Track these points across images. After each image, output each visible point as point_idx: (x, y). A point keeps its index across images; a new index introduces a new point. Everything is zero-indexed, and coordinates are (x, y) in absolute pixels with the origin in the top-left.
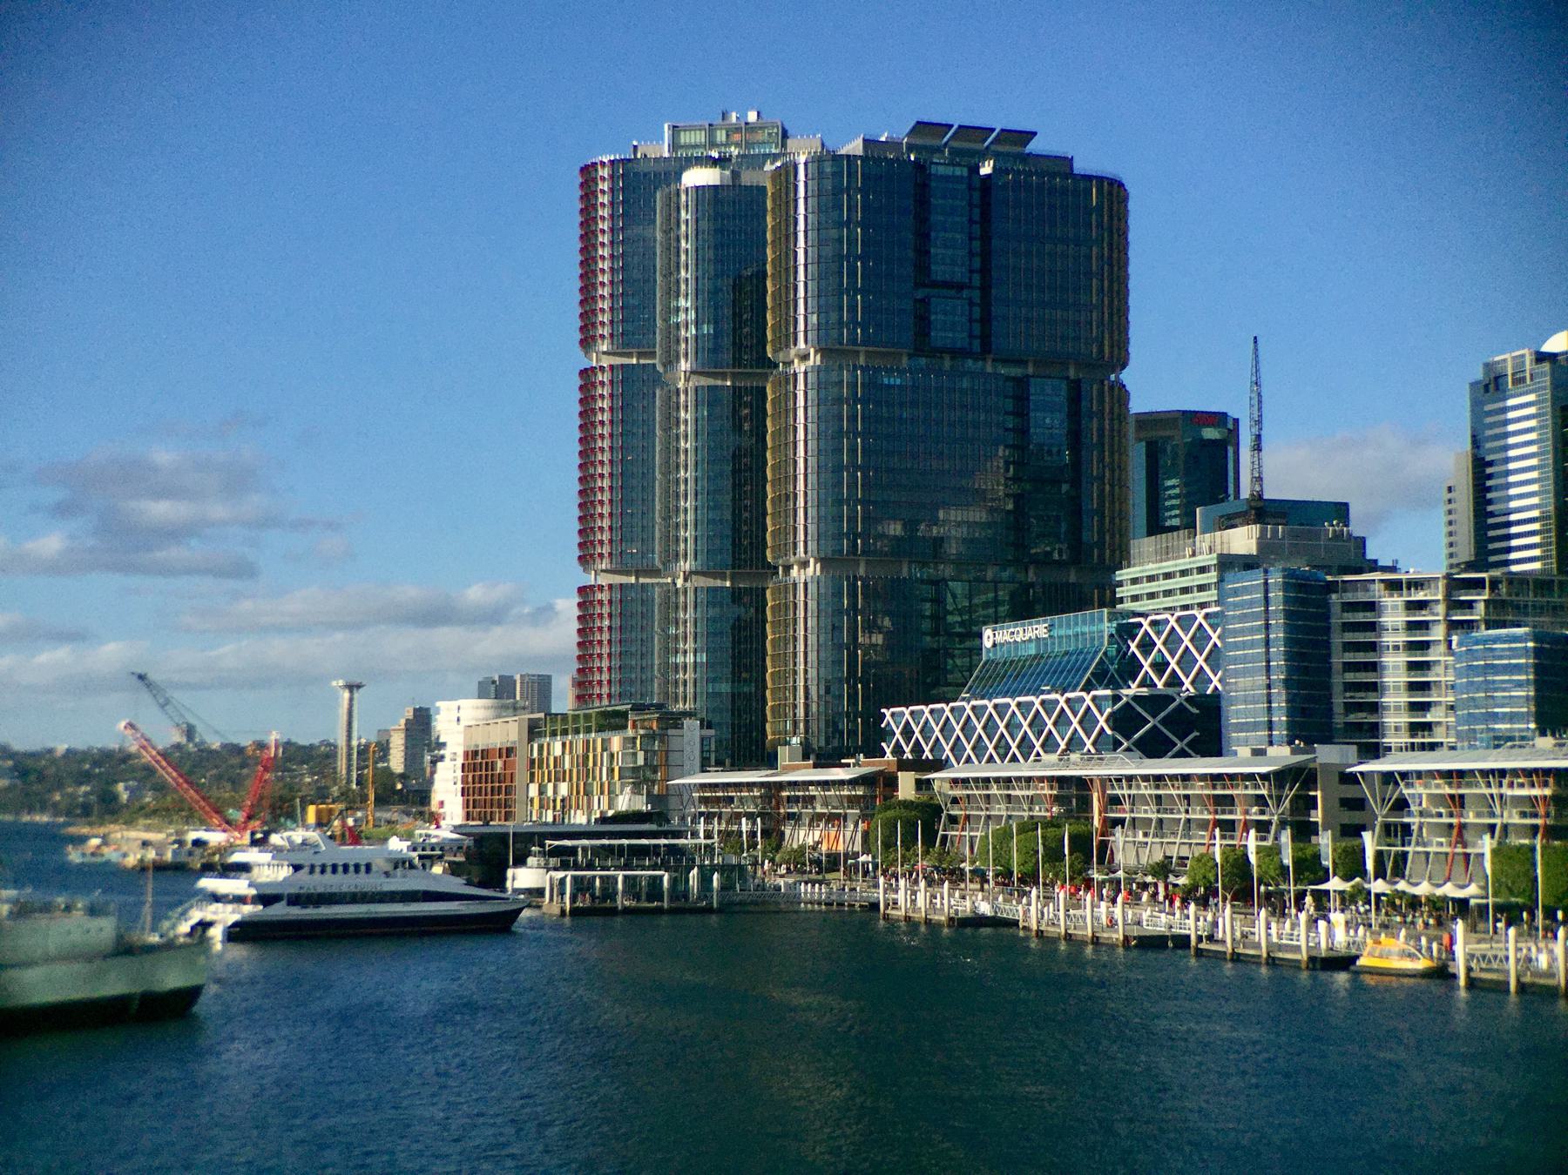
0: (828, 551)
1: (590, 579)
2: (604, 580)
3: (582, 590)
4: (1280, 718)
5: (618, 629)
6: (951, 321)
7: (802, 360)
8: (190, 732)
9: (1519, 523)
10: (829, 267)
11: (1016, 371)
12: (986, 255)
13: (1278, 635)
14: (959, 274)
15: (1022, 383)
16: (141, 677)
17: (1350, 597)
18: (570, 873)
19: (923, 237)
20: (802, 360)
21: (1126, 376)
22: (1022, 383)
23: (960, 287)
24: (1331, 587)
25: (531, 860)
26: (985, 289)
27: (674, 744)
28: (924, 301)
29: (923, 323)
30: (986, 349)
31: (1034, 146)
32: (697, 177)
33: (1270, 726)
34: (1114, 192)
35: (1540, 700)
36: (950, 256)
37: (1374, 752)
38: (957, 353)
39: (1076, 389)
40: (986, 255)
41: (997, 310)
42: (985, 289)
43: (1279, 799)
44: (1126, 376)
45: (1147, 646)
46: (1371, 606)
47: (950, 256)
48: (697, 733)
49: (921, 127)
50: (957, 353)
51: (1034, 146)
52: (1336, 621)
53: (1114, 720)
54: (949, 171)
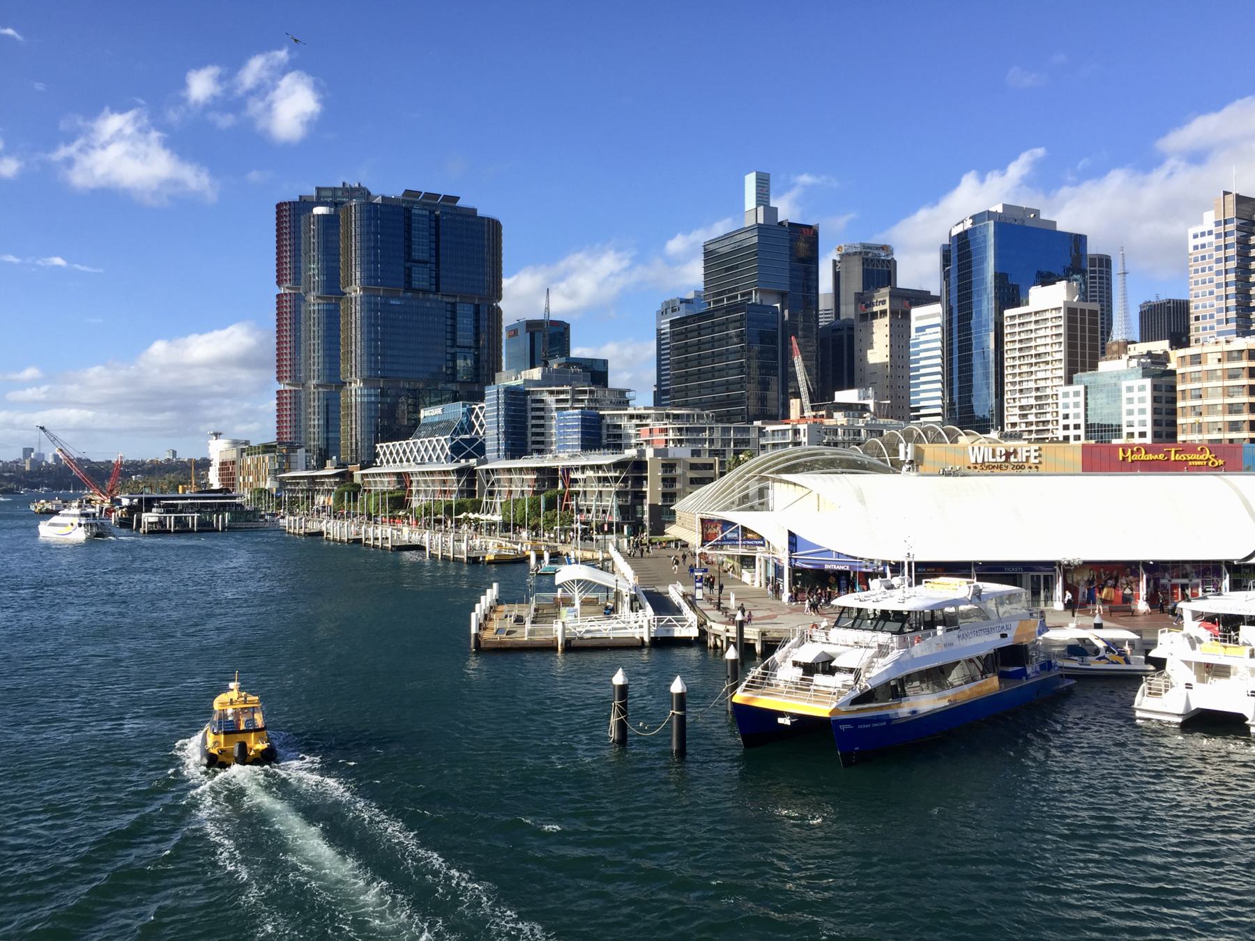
0: (365, 373)
1: (282, 387)
2: (287, 388)
3: (278, 392)
4: (502, 447)
5: (289, 407)
6: (421, 278)
7: (355, 291)
8: (174, 453)
9: (924, 367)
10: (983, 260)
11: (451, 300)
12: (437, 249)
13: (502, 412)
14: (425, 256)
15: (454, 304)
16: (42, 428)
17: (534, 397)
18: (173, 515)
19: (408, 239)
20: (355, 291)
21: (501, 304)
22: (454, 304)
23: (426, 263)
24: (528, 393)
25: (154, 510)
26: (437, 264)
27: (293, 459)
28: (409, 269)
29: (409, 275)
30: (437, 290)
31: (459, 203)
32: (319, 210)
33: (498, 450)
34: (494, 227)
35: (583, 440)
36: (421, 250)
37: (485, 462)
38: (425, 291)
39: (477, 307)
40: (437, 249)
41: (442, 273)
42: (437, 264)
43: (459, 481)
44: (501, 304)
45: (477, 417)
46: (542, 401)
47: (421, 250)
48: (304, 454)
49: (407, 193)
50: (425, 291)
51: (459, 203)
52: (529, 407)
53: (451, 448)
54: (421, 212)
